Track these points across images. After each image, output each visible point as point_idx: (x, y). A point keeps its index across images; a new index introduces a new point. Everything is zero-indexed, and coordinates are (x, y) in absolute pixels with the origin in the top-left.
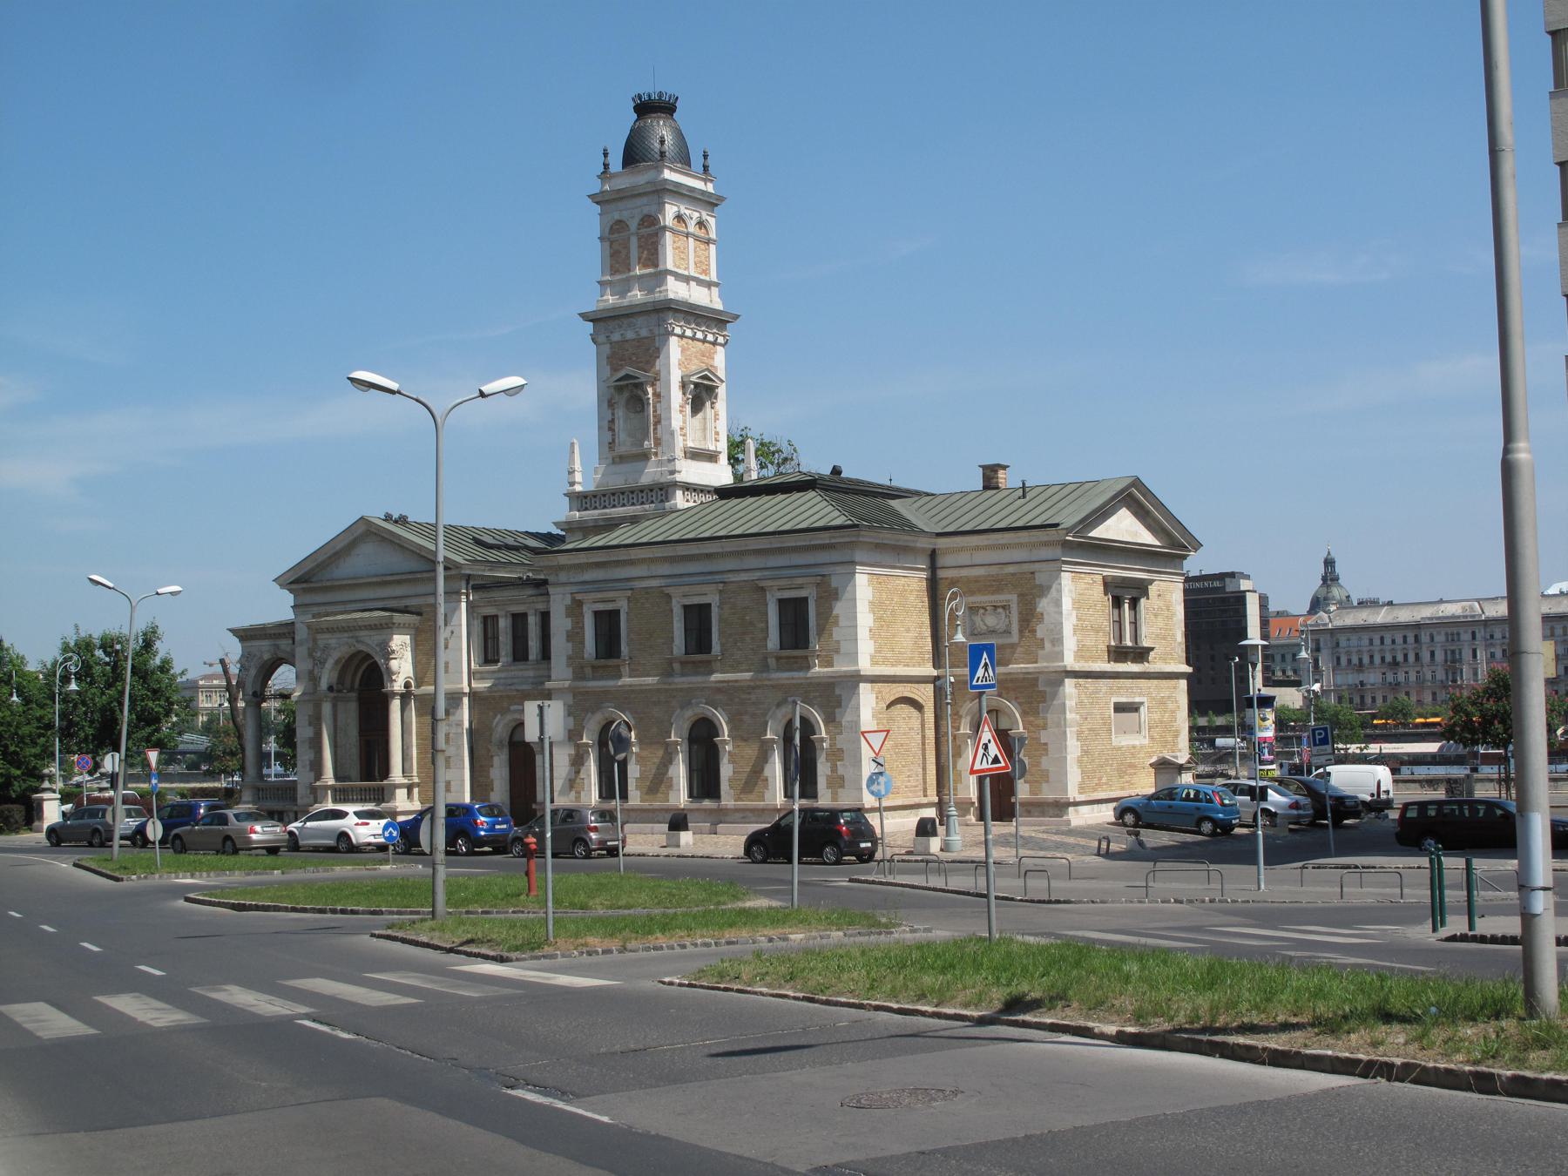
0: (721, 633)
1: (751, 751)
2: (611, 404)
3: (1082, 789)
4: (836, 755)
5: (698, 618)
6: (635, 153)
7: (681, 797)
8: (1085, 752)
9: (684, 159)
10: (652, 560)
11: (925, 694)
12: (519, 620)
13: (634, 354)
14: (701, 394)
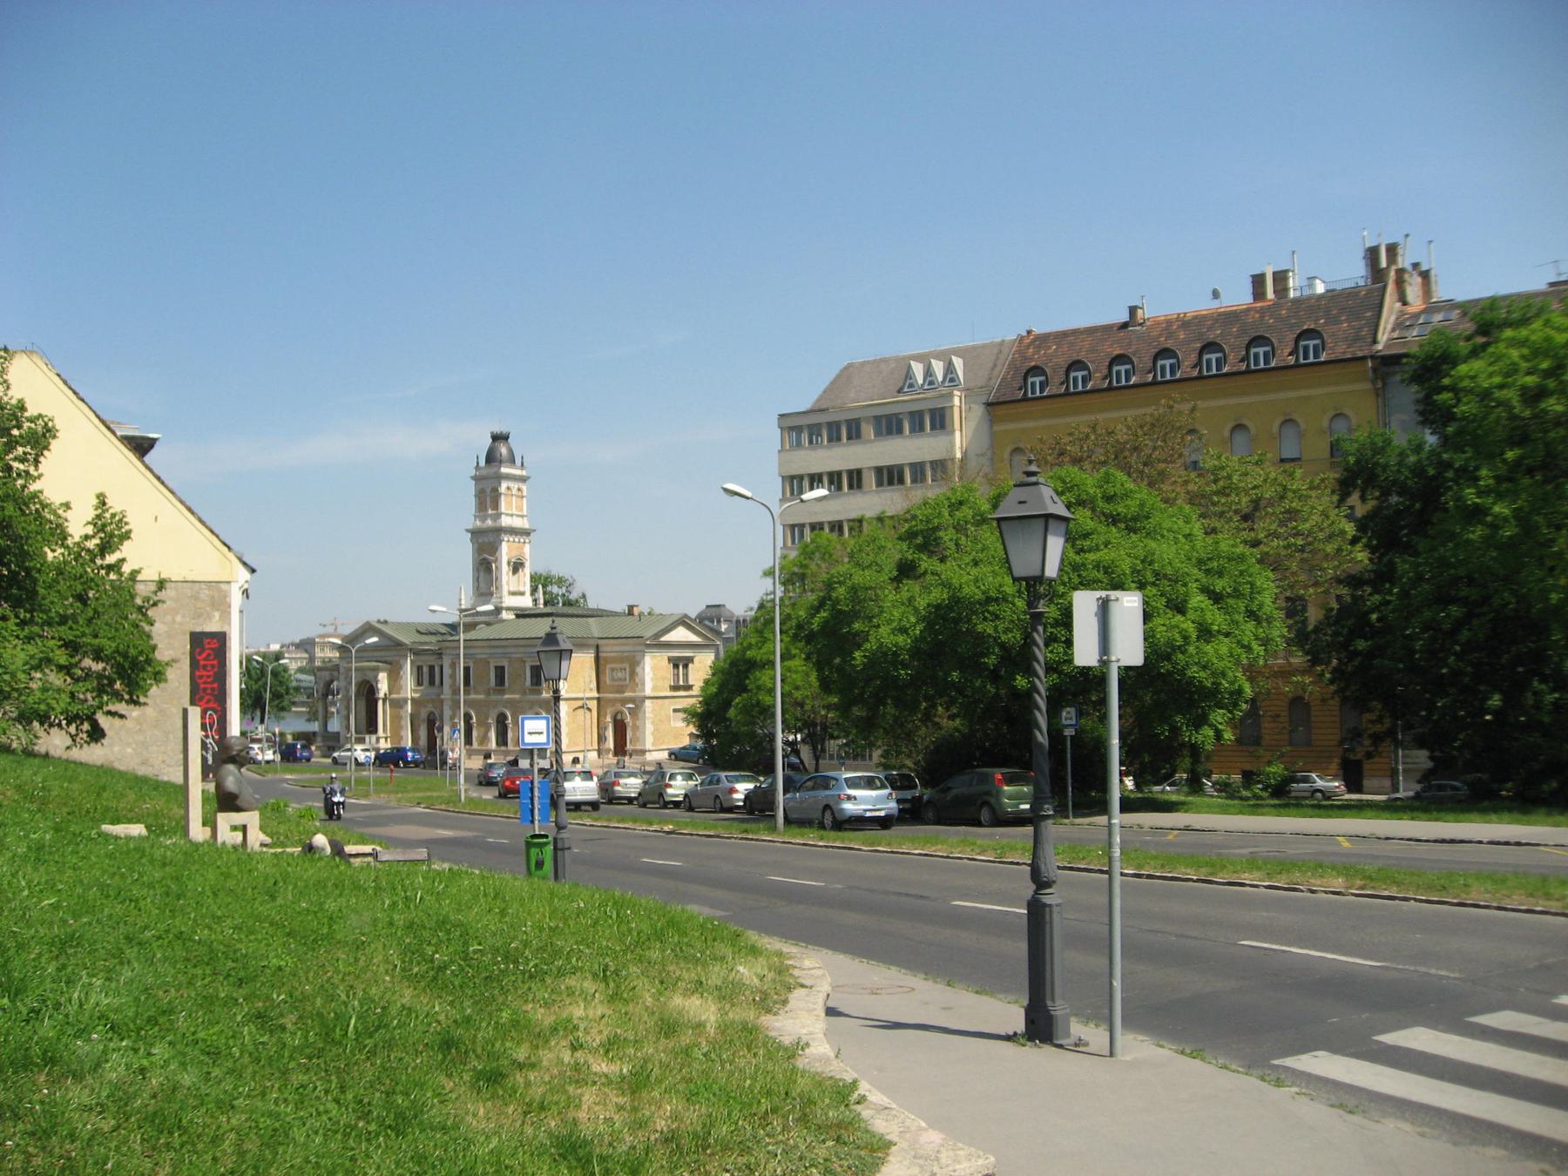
1: (483, 730)
2: (478, 570)
3: (653, 745)
4: (635, 728)
5: (500, 671)
6: (491, 458)
7: (493, 745)
8: (656, 730)
9: (512, 461)
10: (483, 647)
11: (593, 705)
12: (432, 668)
14: (517, 567)
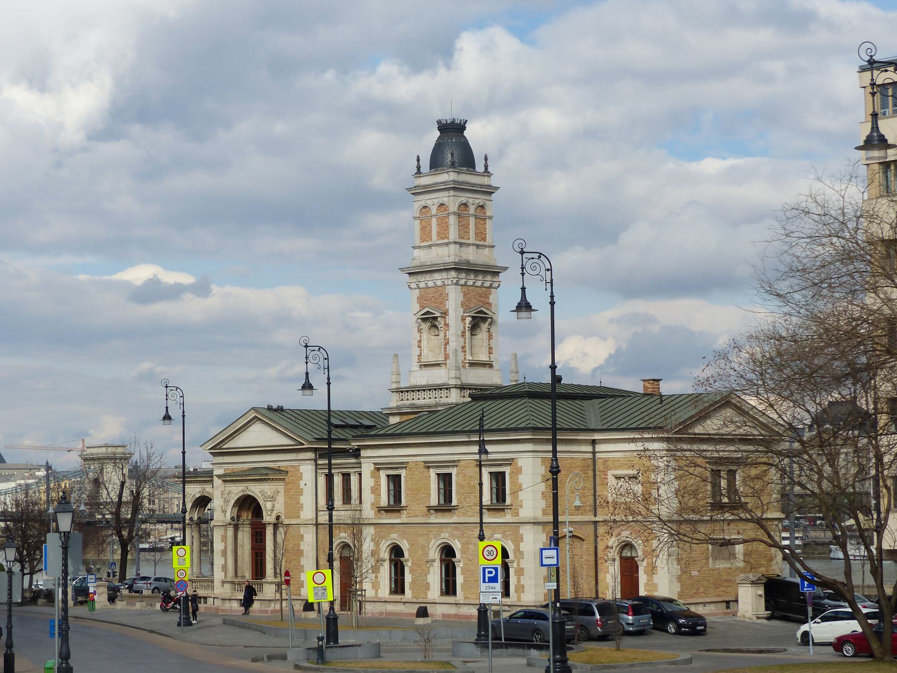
0: (458, 492)
13: (433, 297)
